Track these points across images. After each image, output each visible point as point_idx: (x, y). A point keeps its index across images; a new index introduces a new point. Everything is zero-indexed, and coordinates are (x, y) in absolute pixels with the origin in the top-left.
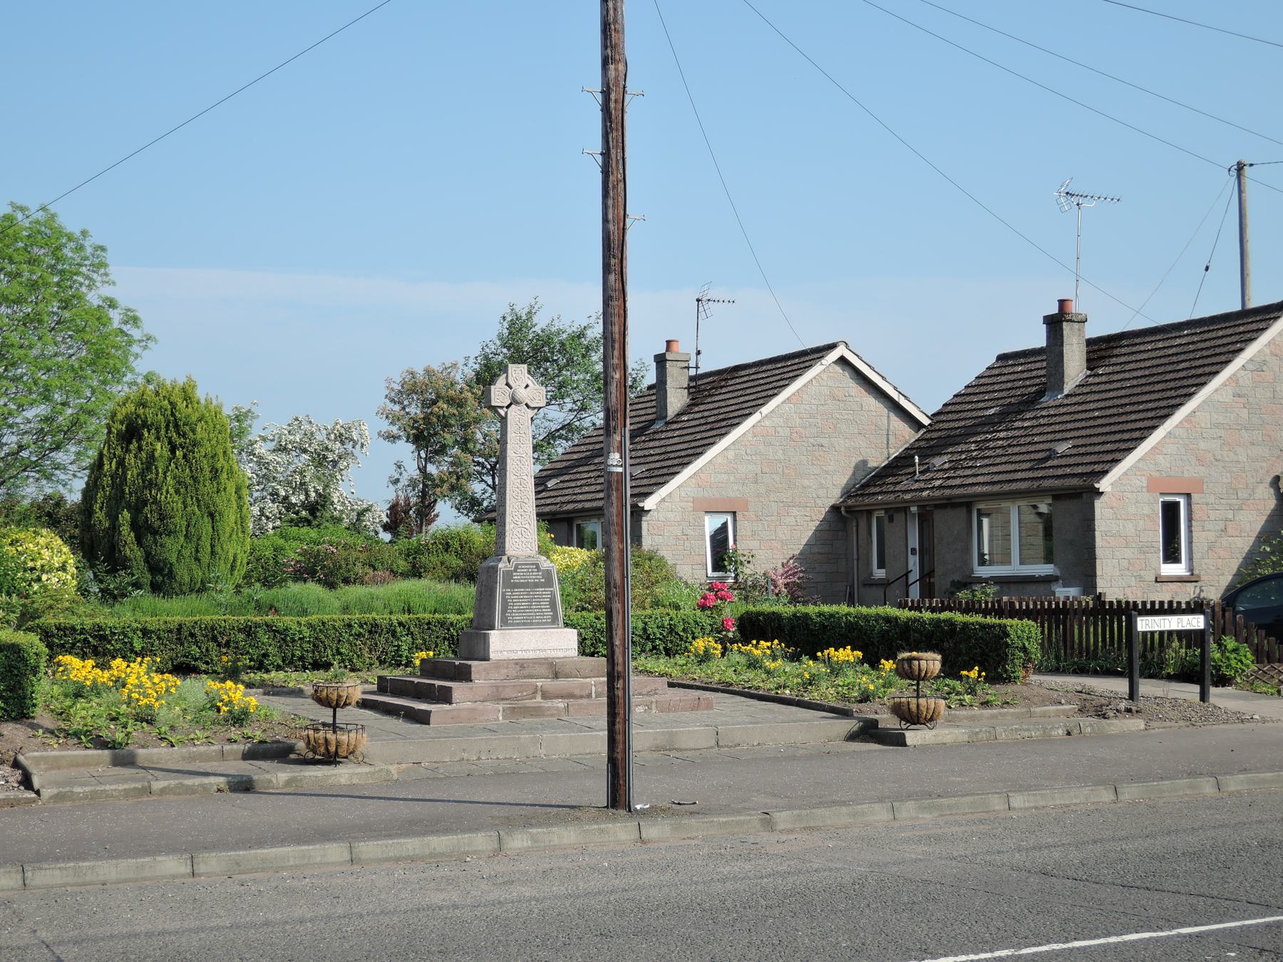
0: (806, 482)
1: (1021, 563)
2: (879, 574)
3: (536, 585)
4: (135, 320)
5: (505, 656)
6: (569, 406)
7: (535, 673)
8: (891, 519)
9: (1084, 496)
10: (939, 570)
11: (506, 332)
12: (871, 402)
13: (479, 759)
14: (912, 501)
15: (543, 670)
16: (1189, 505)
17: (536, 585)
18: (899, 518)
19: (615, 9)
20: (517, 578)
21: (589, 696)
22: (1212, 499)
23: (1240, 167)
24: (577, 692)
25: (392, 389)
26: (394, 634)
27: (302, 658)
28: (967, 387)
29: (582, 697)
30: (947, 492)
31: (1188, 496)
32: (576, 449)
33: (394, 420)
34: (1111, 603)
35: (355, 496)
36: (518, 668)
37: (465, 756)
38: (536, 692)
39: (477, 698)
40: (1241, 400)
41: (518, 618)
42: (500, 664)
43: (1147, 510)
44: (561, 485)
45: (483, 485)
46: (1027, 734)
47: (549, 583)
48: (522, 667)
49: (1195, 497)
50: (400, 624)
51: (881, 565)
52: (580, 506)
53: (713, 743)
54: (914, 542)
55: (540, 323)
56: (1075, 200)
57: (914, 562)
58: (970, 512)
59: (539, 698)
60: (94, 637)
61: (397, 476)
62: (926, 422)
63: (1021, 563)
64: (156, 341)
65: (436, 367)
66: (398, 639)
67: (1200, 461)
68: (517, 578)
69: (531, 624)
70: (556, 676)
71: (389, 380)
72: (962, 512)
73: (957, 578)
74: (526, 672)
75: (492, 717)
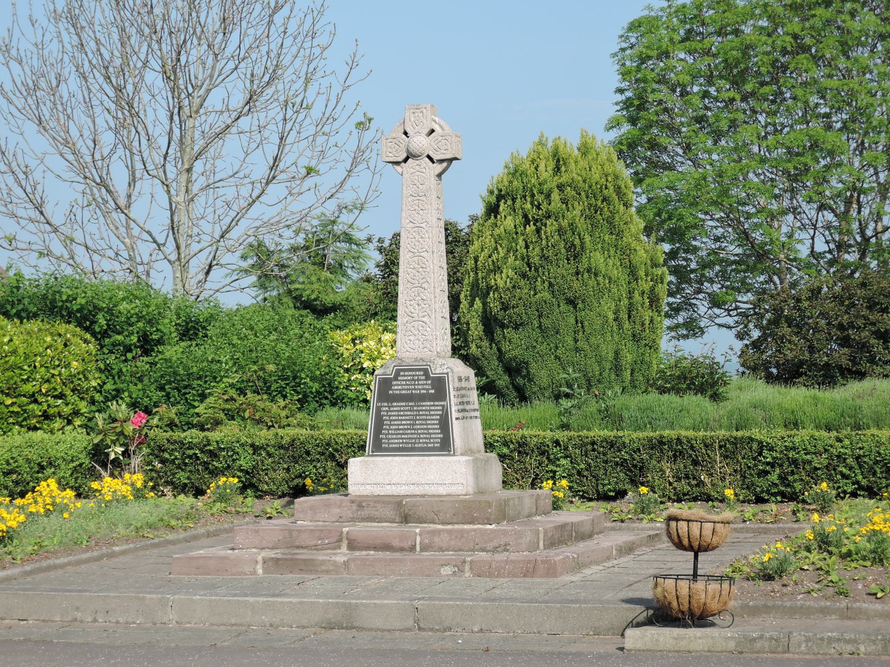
5: (367, 490)
7: (377, 514)
13: (95, 621)
15: (389, 512)
20: (397, 388)
21: (412, 548)
24: (396, 543)
29: (402, 549)
36: (354, 507)
37: (79, 615)
38: (340, 540)
41: (395, 442)
42: (361, 503)
46: (849, 648)
48: (360, 506)
50: (557, 443)
53: (410, 623)
60: (202, 452)
68: (397, 388)
69: (413, 449)
70: (406, 519)
74: (365, 513)
75: (247, 569)
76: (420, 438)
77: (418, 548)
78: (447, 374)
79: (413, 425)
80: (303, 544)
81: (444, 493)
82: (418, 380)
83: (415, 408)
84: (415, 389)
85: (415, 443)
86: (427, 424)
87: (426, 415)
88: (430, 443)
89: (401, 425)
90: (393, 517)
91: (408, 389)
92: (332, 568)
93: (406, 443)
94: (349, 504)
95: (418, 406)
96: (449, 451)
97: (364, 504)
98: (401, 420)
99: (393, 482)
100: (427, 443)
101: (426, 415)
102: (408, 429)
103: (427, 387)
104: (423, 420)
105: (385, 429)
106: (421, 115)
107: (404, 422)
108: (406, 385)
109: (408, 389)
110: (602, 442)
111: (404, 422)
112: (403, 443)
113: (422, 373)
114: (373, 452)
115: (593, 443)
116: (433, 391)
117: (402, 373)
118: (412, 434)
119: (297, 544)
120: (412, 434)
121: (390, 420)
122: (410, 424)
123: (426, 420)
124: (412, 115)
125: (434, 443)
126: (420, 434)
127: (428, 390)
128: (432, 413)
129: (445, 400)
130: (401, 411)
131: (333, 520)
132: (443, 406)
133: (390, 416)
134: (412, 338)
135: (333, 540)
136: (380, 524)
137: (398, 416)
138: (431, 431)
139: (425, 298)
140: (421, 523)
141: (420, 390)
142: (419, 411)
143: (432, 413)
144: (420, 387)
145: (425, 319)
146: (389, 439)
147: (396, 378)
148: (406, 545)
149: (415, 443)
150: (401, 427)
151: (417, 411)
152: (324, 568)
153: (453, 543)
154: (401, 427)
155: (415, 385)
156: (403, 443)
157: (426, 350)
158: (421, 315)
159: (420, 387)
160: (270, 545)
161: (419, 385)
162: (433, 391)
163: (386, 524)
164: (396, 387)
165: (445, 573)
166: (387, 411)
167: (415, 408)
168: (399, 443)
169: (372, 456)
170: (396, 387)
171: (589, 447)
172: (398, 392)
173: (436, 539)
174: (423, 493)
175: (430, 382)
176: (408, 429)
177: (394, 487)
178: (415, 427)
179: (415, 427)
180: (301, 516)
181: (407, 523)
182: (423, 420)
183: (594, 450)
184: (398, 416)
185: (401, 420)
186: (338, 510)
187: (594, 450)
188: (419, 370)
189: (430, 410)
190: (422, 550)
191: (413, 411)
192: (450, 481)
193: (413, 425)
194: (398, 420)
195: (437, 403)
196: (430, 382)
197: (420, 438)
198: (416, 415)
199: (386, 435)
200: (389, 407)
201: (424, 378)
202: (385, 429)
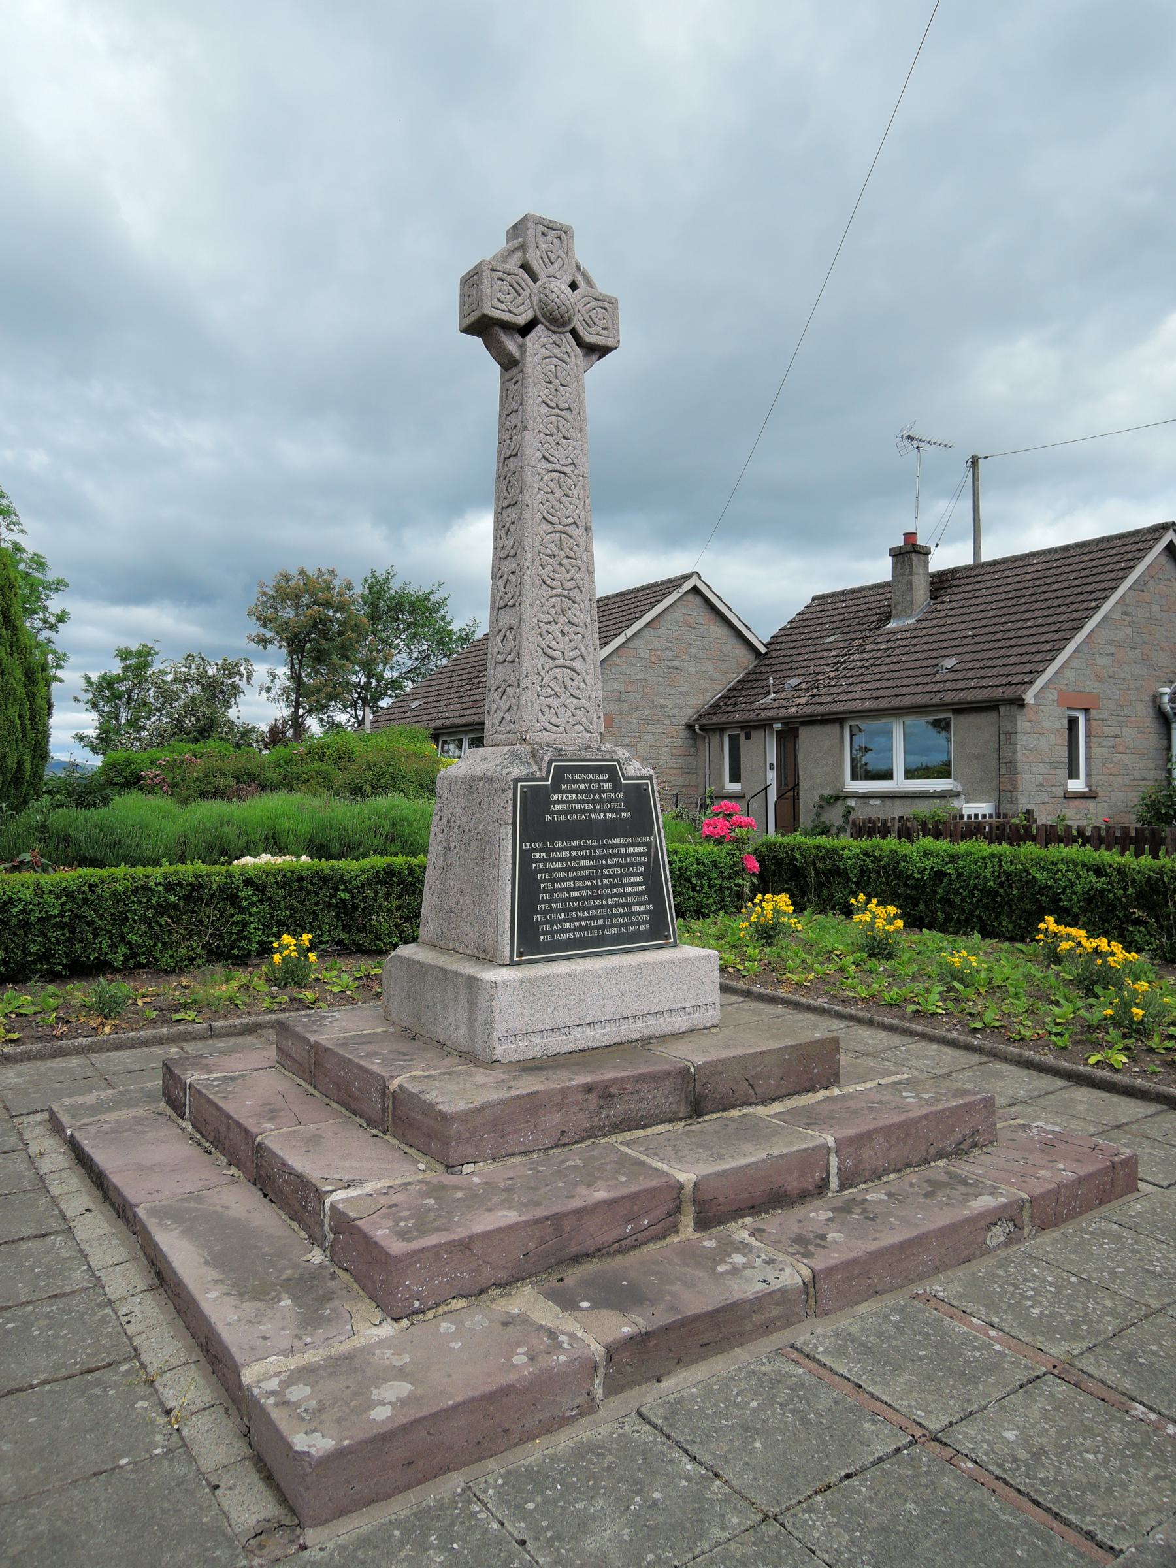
0: (663, 702)
1: (907, 778)
2: (735, 787)
3: (611, 829)
4: (42, 566)
6: (415, 655)
8: (748, 737)
9: (1002, 709)
10: (804, 785)
11: (366, 592)
12: (717, 630)
14: (776, 720)
16: (1087, 720)
17: (611, 829)
18: (757, 735)
19: (199, 1144)
20: (560, 810)
22: (1105, 715)
23: (974, 462)
24: (792, 1184)
25: (265, 594)
26: (234, 899)
27: (45, 957)
28: (791, 622)
30: (813, 707)
31: (1086, 710)
32: (419, 690)
33: (265, 622)
34: (969, 817)
35: (240, 721)
36: (593, 1101)
39: (488, 1275)
40: (1128, 618)
41: (565, 928)
43: (1058, 726)
44: (425, 706)
45: (347, 716)
47: (641, 823)
49: (1093, 712)
51: (735, 777)
52: (448, 722)
54: (772, 758)
55: (395, 585)
56: (915, 443)
57: (772, 777)
58: (842, 728)
59: (687, 1231)
61: (269, 684)
62: (763, 650)
63: (907, 778)
64: (67, 586)
65: (311, 571)
66: (242, 910)
67: (1099, 678)
68: (560, 810)
69: (600, 941)
71: (262, 585)
72: (837, 726)
73: (827, 792)
74: (617, 1110)
76: (612, 916)
77: (834, 1183)
78: (650, 778)
79: (598, 888)
80: (589, 1245)
81: (683, 1029)
82: (601, 791)
83: (599, 852)
84: (595, 811)
85: (603, 927)
86: (623, 886)
87: (621, 866)
88: (632, 924)
89: (575, 889)
90: (674, 1107)
91: (581, 812)
92: (776, 1311)
93: (587, 928)
94: (580, 1097)
95: (604, 847)
96: (667, 937)
97: (614, 1091)
98: (575, 879)
99: (589, 1019)
100: (626, 925)
101: (621, 866)
102: (588, 898)
103: (616, 806)
104: (615, 876)
105: (544, 901)
106: (556, 242)
107: (579, 884)
108: (578, 801)
109: (581, 812)
110: (313, 877)
111: (579, 884)
112: (581, 929)
113: (605, 776)
114: (521, 954)
115: (301, 879)
116: (628, 815)
117: (568, 776)
118: (596, 907)
119: (574, 1249)
120: (596, 907)
121: (553, 881)
122: (591, 888)
123: (621, 876)
124: (541, 240)
125: (638, 923)
126: (611, 907)
127: (619, 812)
128: (631, 860)
129: (650, 832)
130: (572, 859)
131: (548, 1143)
132: (648, 845)
133: (551, 871)
134: (554, 702)
135: (659, 1213)
136: (649, 1131)
137: (567, 869)
138: (631, 899)
139: (575, 620)
140: (725, 1110)
141: (605, 811)
142: (606, 857)
143: (631, 860)
144: (604, 806)
145: (575, 664)
146: (551, 923)
147: (556, 787)
148: (810, 1183)
149: (603, 927)
150: (575, 894)
151: (602, 857)
152: (757, 1318)
153: (893, 1153)
154: (575, 894)
155: (594, 802)
156: (581, 929)
157: (579, 728)
158: (569, 655)
159: (604, 806)
160: (503, 1275)
161: (601, 801)
162: (628, 815)
163: (661, 1128)
164: (558, 807)
165: (995, 1242)
166: (544, 861)
167: (599, 852)
168: (574, 930)
169: (519, 963)
170: (558, 807)
171: (296, 886)
172: (562, 817)
173: (866, 1153)
174: (646, 1033)
175: (621, 795)
176: (588, 898)
177: (589, 1032)
178: (602, 892)
179: (602, 892)
180: (470, 1151)
181: (700, 1116)
182: (615, 876)
183: (301, 889)
184: (567, 869)
185: (575, 879)
186: (557, 1117)
187: (301, 889)
188: (600, 769)
189: (627, 855)
190: (843, 1187)
191: (595, 857)
192: (694, 1002)
193: (598, 888)
194: (567, 879)
195: (637, 840)
196: (621, 795)
197: (612, 916)
198: (602, 867)
199: (546, 913)
200: (548, 851)
201: (608, 786)
202: (544, 901)
